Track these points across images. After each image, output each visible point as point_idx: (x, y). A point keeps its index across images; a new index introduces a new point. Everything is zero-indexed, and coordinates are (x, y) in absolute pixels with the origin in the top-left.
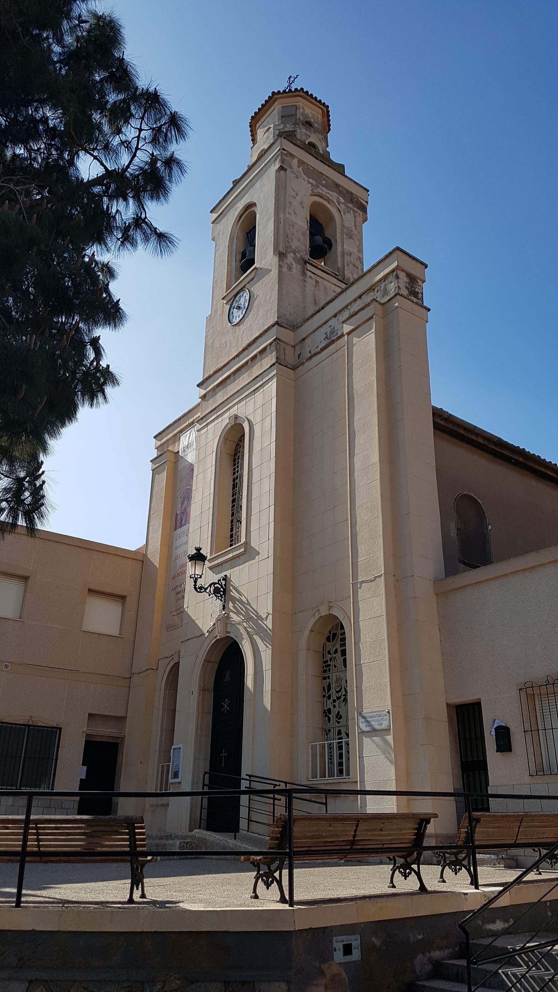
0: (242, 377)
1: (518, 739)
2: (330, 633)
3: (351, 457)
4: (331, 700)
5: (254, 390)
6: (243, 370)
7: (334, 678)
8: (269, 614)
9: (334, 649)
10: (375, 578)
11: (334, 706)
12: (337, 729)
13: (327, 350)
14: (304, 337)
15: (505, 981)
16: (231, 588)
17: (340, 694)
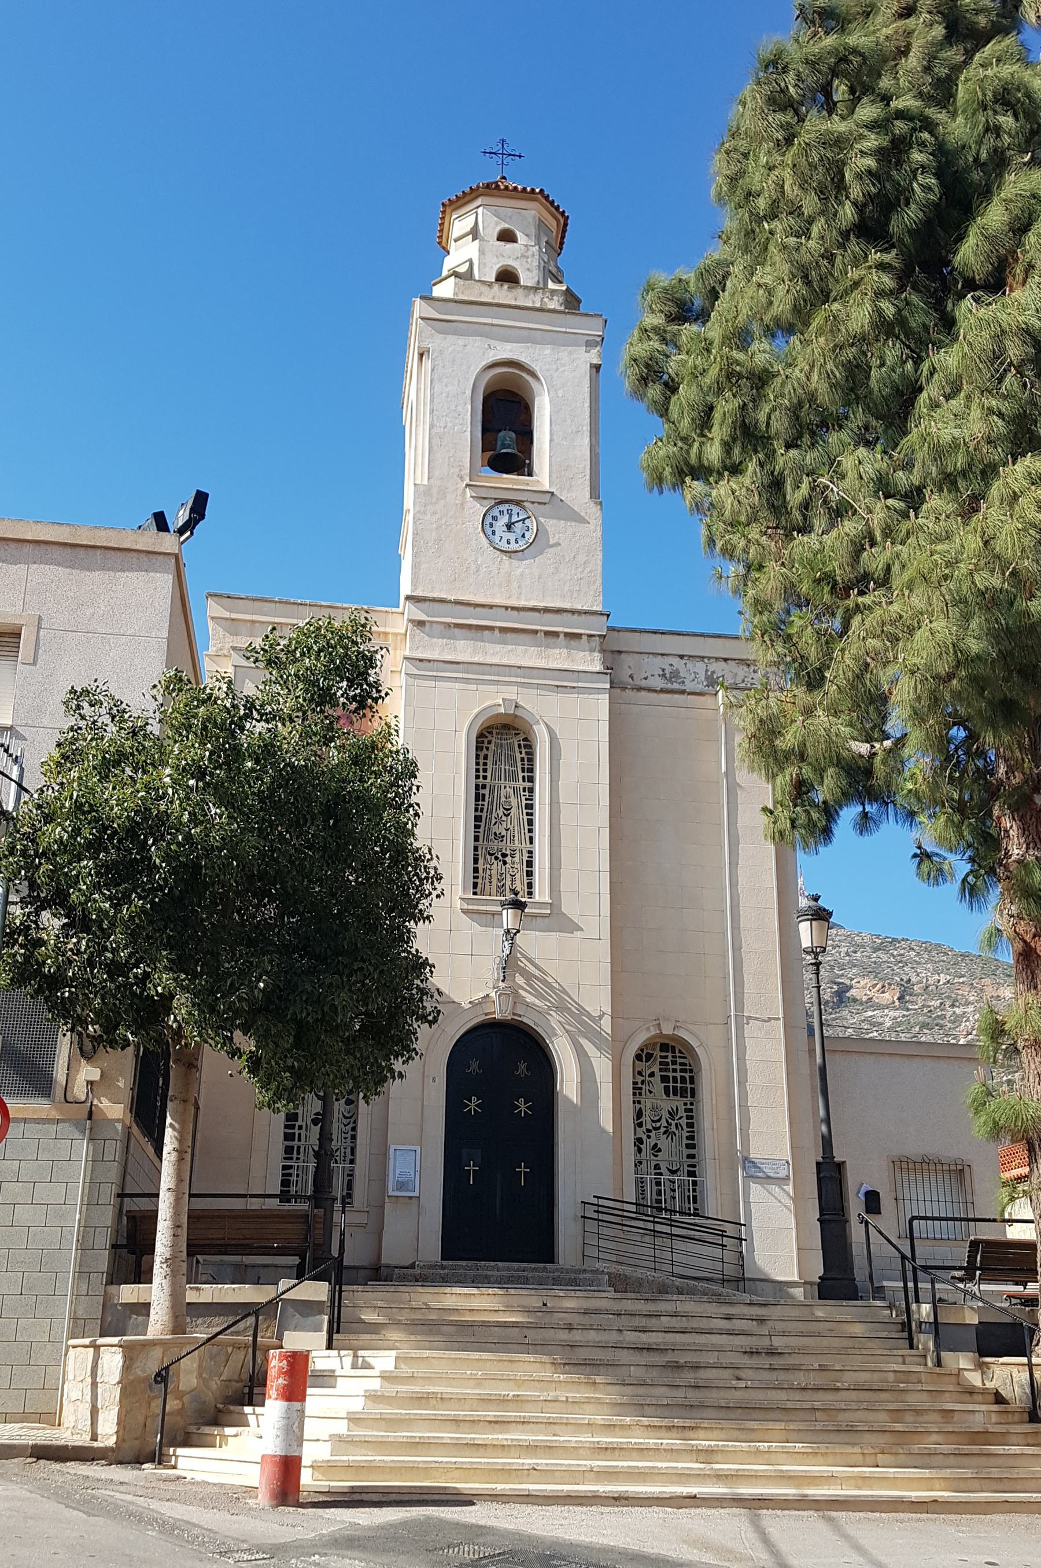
0: (510, 647)
1: (886, 1202)
2: (642, 1050)
3: (734, 864)
4: (644, 1128)
5: (558, 686)
6: (522, 637)
7: (649, 1105)
8: (604, 1014)
9: (649, 1072)
10: (770, 1019)
11: (649, 1137)
12: (653, 1163)
13: (669, 696)
14: (621, 649)
15: (436, 1432)
16: (519, 955)
17: (658, 1125)
